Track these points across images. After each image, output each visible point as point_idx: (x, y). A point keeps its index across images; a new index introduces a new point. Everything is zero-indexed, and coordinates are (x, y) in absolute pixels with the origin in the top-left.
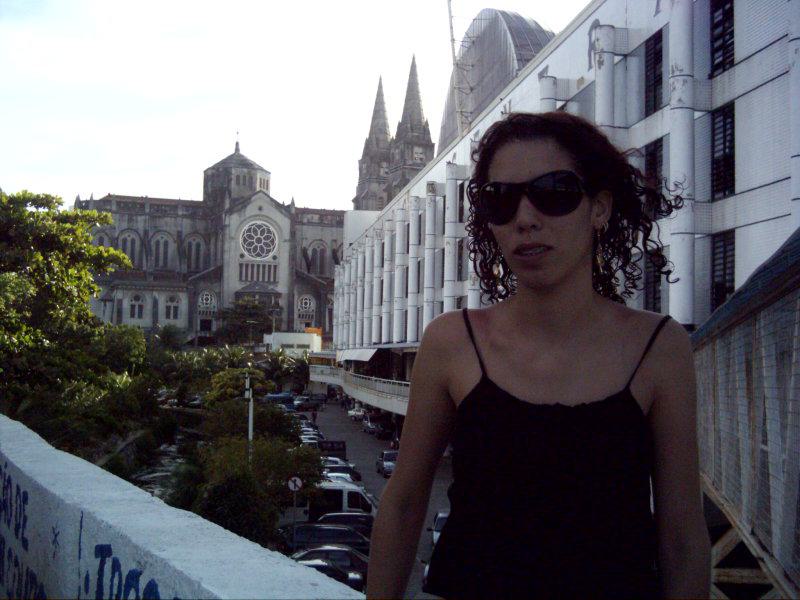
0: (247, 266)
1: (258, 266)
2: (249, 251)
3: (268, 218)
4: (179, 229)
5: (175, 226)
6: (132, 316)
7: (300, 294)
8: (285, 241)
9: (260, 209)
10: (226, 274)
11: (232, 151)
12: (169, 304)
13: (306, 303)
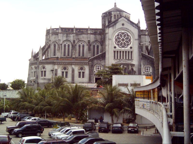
0: (118, 52)
1: (123, 52)
2: (118, 45)
3: (127, 29)
4: (89, 39)
5: (88, 38)
6: (80, 77)
7: (144, 65)
8: (136, 40)
10: (107, 56)
11: (113, 6)
12: (80, 71)
13: (147, 69)
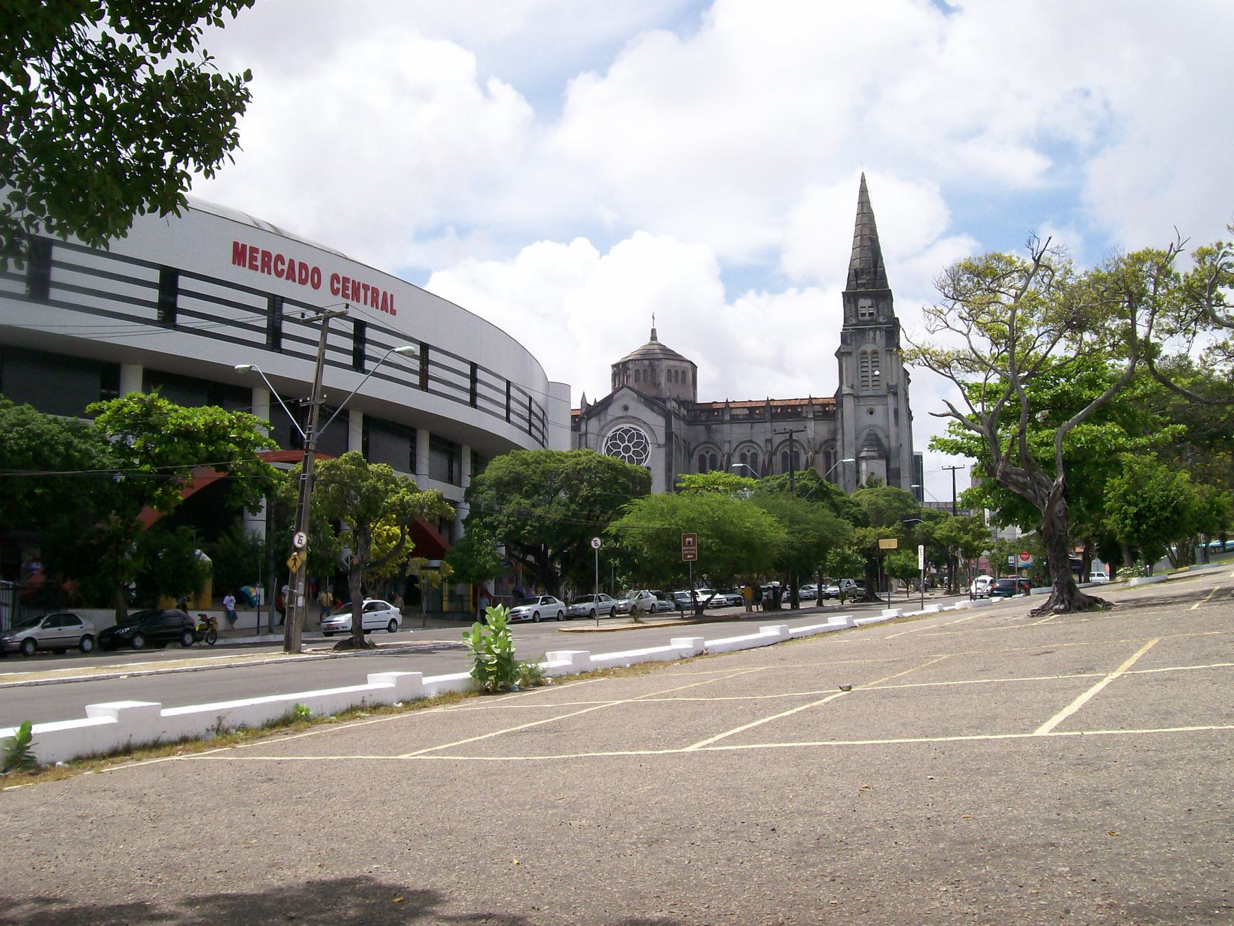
3: (635, 419)
9: (626, 408)
